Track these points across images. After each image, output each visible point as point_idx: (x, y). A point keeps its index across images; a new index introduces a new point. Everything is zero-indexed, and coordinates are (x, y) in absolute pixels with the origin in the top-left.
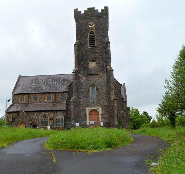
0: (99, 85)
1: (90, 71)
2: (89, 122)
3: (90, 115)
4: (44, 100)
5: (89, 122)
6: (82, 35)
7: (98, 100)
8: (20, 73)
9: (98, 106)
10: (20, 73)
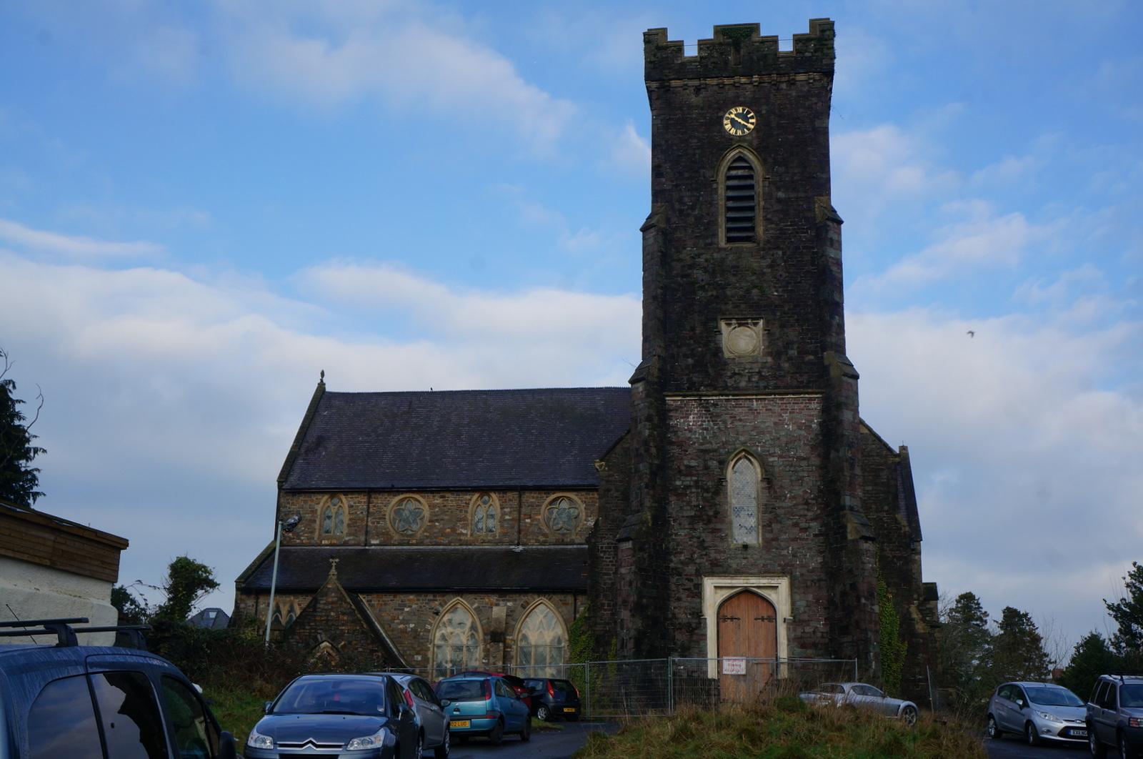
0: (780, 457)
1: (729, 374)
2: (720, 664)
3: (725, 619)
4: (454, 530)
5: (720, 664)
6: (686, 175)
7: (769, 536)
8: (323, 374)
9: (765, 572)
10: (323, 374)
